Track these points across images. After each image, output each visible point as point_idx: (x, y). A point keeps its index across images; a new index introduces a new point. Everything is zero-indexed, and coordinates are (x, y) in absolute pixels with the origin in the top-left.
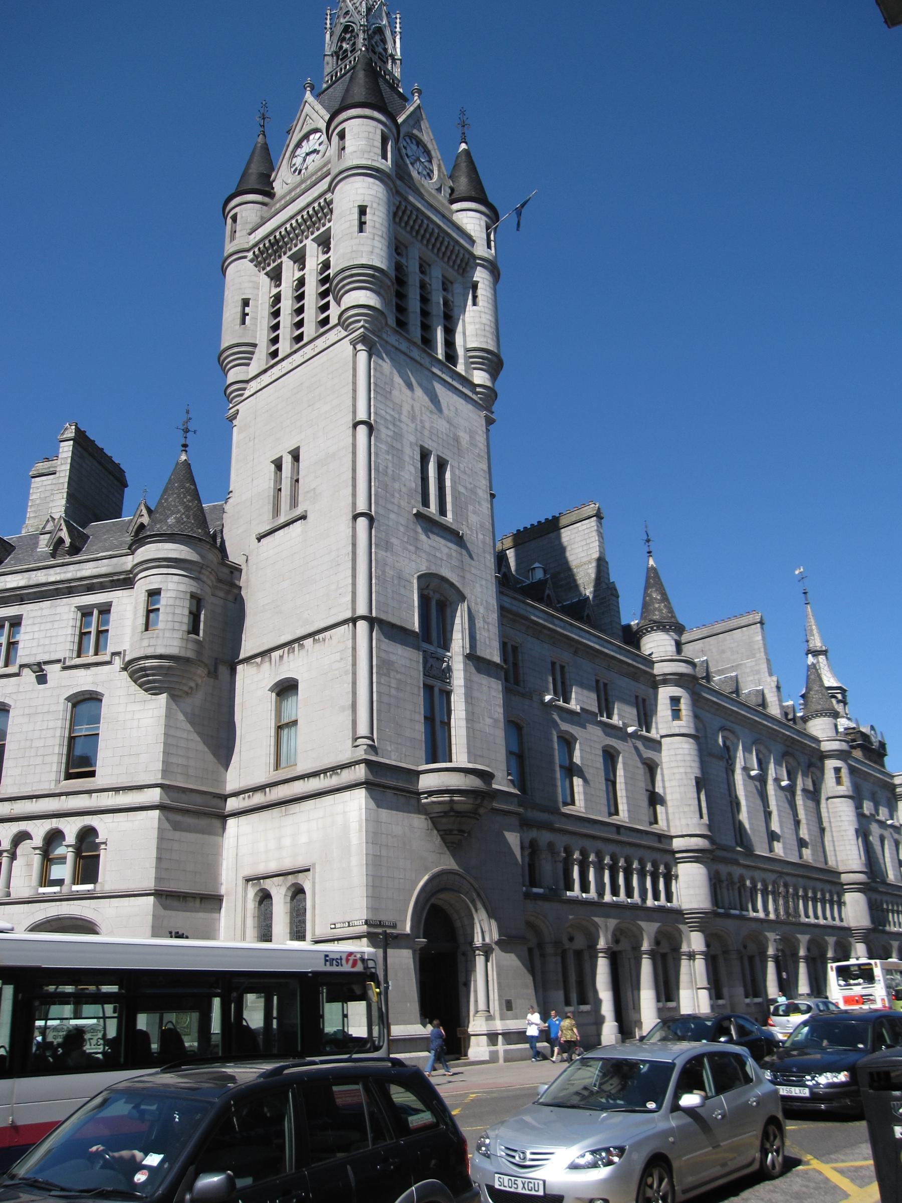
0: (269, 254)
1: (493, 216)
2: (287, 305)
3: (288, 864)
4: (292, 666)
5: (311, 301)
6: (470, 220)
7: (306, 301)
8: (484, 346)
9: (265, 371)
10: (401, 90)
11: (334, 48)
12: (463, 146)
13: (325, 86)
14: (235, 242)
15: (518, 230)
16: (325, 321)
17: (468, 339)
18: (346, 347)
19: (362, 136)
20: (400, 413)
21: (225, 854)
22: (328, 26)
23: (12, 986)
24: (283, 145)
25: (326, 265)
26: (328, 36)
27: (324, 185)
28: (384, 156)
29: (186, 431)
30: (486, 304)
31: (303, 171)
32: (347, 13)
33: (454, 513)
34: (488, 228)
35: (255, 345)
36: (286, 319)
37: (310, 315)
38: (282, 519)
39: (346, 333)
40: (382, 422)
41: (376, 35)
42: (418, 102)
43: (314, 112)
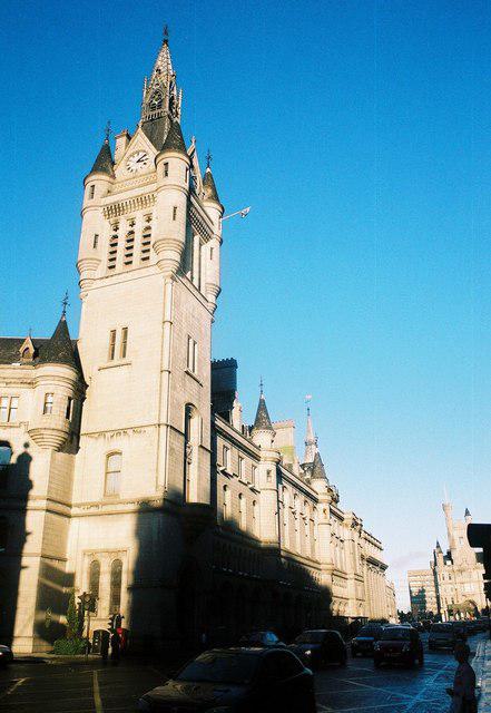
2: (122, 243)
3: (112, 547)
4: (118, 443)
6: (212, 210)
15: (121, 454)
21: (69, 545)
23: (488, 521)
29: (65, 304)
33: (199, 371)
38: (115, 362)
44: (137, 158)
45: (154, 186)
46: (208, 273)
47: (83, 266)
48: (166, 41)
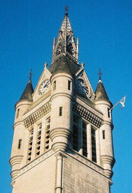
0: (30, 121)
1: (109, 104)
2: (35, 141)
5: (43, 140)
6: (102, 107)
7: (41, 140)
8: (107, 154)
9: (26, 166)
10: (78, 63)
11: (55, 51)
12: (100, 81)
13: (52, 63)
14: (18, 119)
16: (47, 147)
17: (101, 152)
18: (53, 158)
19: (63, 80)
20: (74, 183)
22: (54, 44)
24: (36, 84)
25: (49, 127)
26: (54, 47)
27: (48, 99)
28: (69, 89)
30: (108, 138)
31: (43, 93)
32: (60, 39)
34: (108, 110)
35: (22, 156)
36: (34, 147)
37: (43, 145)
39: (54, 152)
40: (66, 187)
41: (69, 48)
42: (83, 68)
43: (47, 74)
44: (44, 85)
45: (48, 99)
46: (102, 148)
47: (13, 161)
48: (67, 15)
